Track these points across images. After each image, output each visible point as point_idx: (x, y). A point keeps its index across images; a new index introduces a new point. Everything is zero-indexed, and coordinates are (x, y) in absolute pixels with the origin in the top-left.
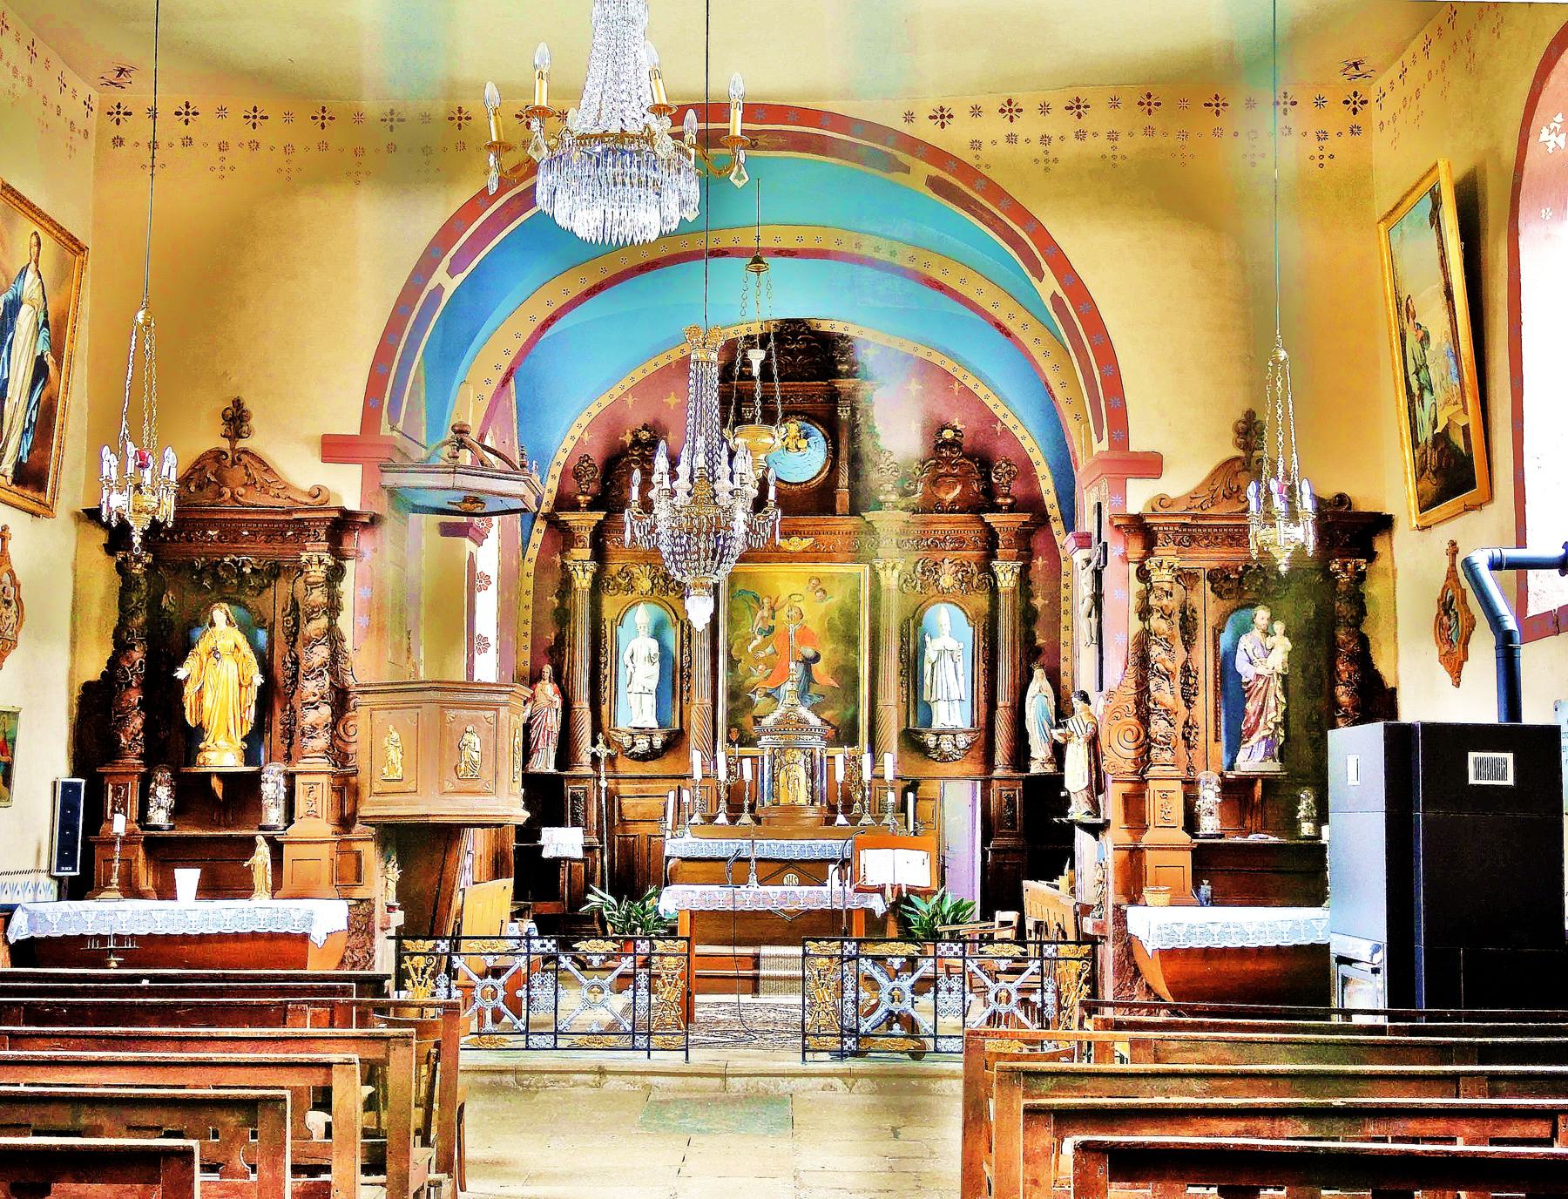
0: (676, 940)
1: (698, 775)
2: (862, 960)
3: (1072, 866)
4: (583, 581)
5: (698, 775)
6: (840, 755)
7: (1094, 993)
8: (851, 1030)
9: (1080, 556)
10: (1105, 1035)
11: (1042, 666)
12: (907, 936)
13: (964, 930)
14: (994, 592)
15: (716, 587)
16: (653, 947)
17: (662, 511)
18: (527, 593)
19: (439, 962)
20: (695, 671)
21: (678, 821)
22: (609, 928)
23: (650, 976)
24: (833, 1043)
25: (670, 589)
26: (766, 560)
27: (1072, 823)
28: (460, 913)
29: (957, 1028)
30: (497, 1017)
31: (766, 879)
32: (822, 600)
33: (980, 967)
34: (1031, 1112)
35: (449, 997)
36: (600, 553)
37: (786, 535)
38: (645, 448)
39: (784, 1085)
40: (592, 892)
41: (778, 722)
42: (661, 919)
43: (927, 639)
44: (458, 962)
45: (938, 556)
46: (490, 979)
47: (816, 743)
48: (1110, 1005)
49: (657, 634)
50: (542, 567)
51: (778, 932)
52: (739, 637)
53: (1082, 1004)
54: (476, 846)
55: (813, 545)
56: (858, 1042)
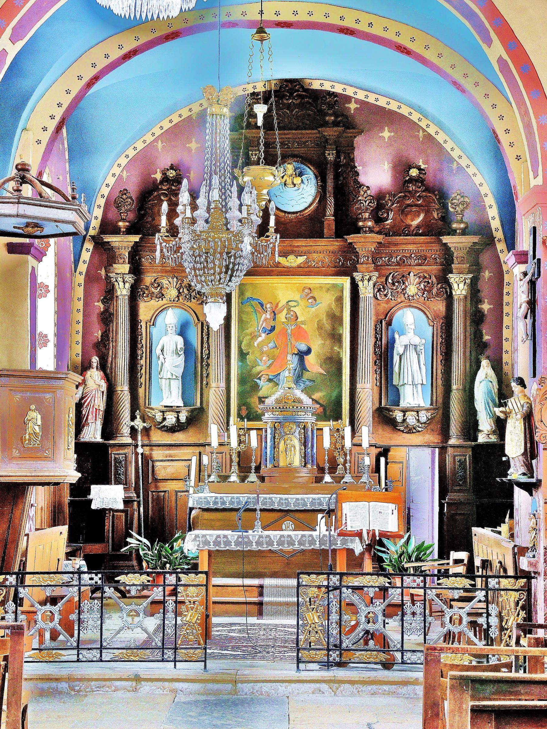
0: (197, 574)
1: (215, 443)
2: (344, 590)
3: (512, 517)
4: (123, 291)
5: (215, 443)
6: (327, 427)
7: (529, 617)
8: (335, 646)
9: (519, 269)
10: (536, 651)
11: (488, 358)
12: (380, 571)
13: (426, 566)
14: (449, 299)
15: (229, 297)
16: (179, 579)
17: (185, 235)
18: (79, 299)
19: (8, 593)
20: (213, 361)
21: (199, 479)
22: (144, 564)
23: (176, 602)
24: (321, 655)
25: (192, 296)
26: (269, 273)
27: (511, 484)
28: (25, 554)
29: (419, 644)
30: (54, 636)
31: (268, 526)
32: (312, 306)
33: (438, 596)
34: (477, 712)
35: (16, 620)
36: (136, 269)
37: (284, 254)
38: (172, 183)
39: (282, 688)
40: (131, 536)
41: (278, 401)
42: (186, 557)
43: (396, 336)
44: (23, 593)
45: (404, 270)
46: (48, 607)
47: (309, 419)
48: (541, 626)
49: (182, 331)
50: (90, 278)
51: (277, 568)
52: (247, 334)
53: (519, 626)
54: (38, 500)
55: (306, 262)
56: (341, 655)
